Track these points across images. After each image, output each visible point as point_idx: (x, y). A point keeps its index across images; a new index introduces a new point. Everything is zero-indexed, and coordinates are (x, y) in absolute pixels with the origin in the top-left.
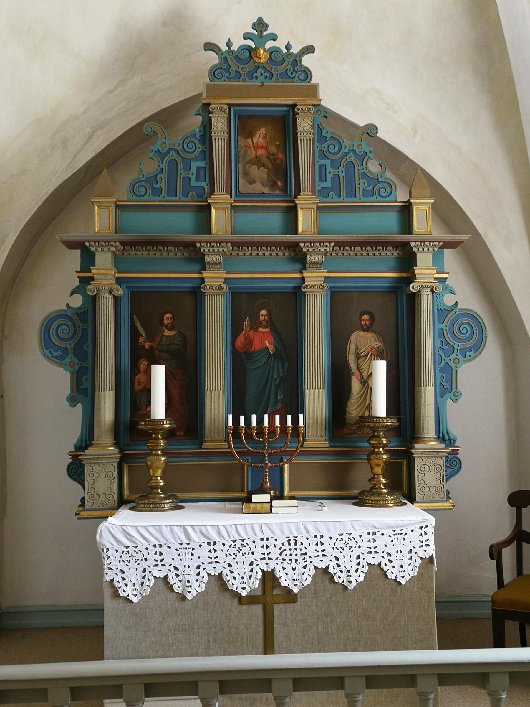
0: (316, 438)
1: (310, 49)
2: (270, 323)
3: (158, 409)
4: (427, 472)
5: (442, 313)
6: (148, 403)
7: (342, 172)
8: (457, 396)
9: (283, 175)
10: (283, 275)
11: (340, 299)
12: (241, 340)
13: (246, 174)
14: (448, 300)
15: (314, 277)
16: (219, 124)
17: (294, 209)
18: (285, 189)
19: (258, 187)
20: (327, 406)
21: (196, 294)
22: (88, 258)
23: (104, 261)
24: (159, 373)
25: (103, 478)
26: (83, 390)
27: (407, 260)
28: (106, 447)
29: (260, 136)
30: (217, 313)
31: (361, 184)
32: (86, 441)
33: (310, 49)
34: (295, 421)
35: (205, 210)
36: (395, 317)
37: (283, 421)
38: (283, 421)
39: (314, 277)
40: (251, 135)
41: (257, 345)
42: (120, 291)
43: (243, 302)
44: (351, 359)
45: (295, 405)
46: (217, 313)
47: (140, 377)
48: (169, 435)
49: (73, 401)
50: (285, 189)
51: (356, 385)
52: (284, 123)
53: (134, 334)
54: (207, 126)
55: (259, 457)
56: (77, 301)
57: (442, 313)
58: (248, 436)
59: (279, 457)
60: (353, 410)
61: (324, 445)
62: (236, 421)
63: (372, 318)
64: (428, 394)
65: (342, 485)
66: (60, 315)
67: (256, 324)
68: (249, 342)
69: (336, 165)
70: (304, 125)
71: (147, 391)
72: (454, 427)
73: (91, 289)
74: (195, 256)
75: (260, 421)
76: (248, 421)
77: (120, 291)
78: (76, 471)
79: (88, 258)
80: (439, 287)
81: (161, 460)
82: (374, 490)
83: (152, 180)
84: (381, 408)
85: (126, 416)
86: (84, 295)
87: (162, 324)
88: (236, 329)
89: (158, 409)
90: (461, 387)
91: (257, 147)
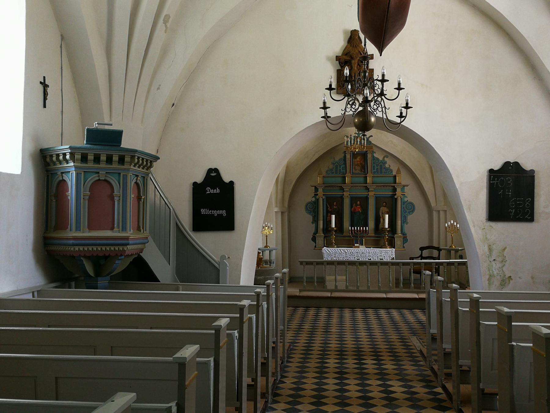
0: (371, 233)
1: (372, 136)
2: (360, 205)
3: (333, 225)
4: (398, 241)
5: (403, 203)
6: (331, 224)
7: (379, 167)
8: (407, 223)
9: (364, 168)
10: (363, 193)
11: (378, 200)
12: (353, 209)
13: (355, 168)
14: (406, 199)
15: (371, 194)
16: (348, 156)
17: (367, 177)
18: (364, 172)
19: (358, 171)
20: (360, 4)
21: (342, 198)
22: (316, 189)
23: (320, 190)
24: (333, 217)
25: (320, 240)
26: (315, 220)
27: (395, 190)
28: (321, 233)
29: (358, 159)
30: (347, 202)
31: (384, 171)
32: (316, 232)
33: (372, 136)
34: (366, 229)
35: (344, 178)
36: (391, 203)
37: (363, 229)
38: (363, 229)
39: (371, 194)
40: (356, 158)
41: (357, 210)
42: (324, 197)
43: (353, 200)
44: (381, 214)
45: (366, 225)
46: (347, 202)
47: (329, 217)
48: (336, 231)
49: (313, 223)
50: (364, 172)
51: (382, 220)
52: (364, 155)
53: (327, 207)
54: (345, 157)
55: (357, 237)
56: (314, 199)
57: (403, 203)
58: (357, 231)
59: (363, 237)
60: (381, 226)
61: (373, 235)
62: (351, 228)
63: (386, 204)
64: (399, 223)
65: (378, 244)
66: (310, 203)
67: (357, 205)
68: (355, 209)
69: (377, 166)
70: (369, 156)
71: (330, 221)
72: (406, 230)
73: (317, 197)
74: (342, 189)
75: (357, 229)
76: (354, 228)
77: (324, 197)
78: (314, 239)
79: (316, 189)
80: (402, 197)
81: (511, 212)
82: (385, 244)
83: (332, 170)
84: (387, 226)
85: (325, 227)
86: (316, 198)
87: (334, 205)
88: (352, 206)
89: (333, 225)
90: (408, 221)
91: (357, 161)
